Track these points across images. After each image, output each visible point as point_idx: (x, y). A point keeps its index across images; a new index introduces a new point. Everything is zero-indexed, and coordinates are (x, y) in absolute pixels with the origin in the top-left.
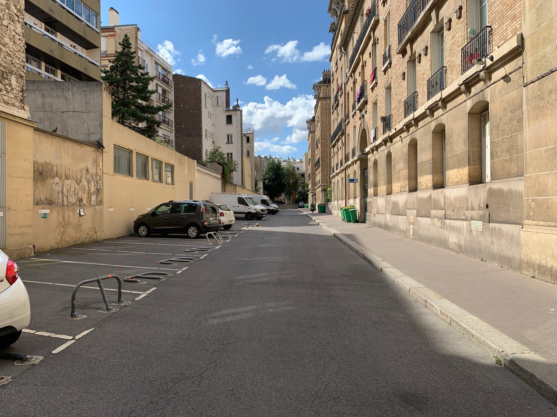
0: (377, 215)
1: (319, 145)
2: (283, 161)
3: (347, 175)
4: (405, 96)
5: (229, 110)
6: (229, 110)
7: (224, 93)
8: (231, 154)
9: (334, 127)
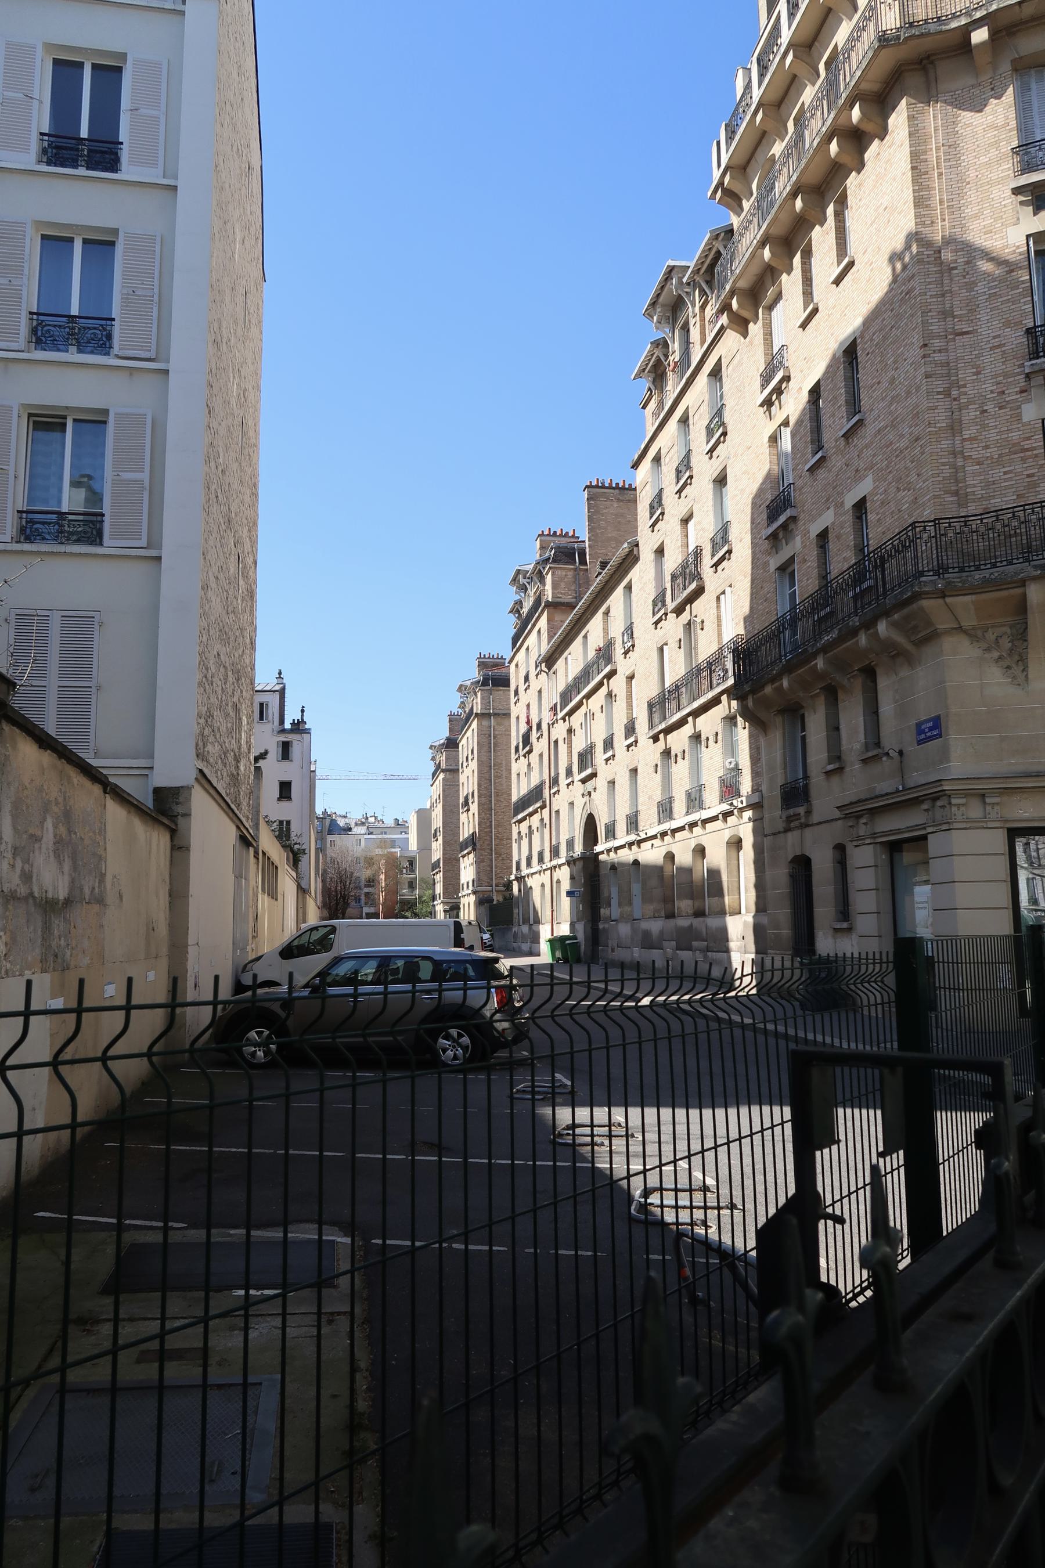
3: (555, 880)
4: (658, 796)
7: (277, 696)
8: (288, 822)
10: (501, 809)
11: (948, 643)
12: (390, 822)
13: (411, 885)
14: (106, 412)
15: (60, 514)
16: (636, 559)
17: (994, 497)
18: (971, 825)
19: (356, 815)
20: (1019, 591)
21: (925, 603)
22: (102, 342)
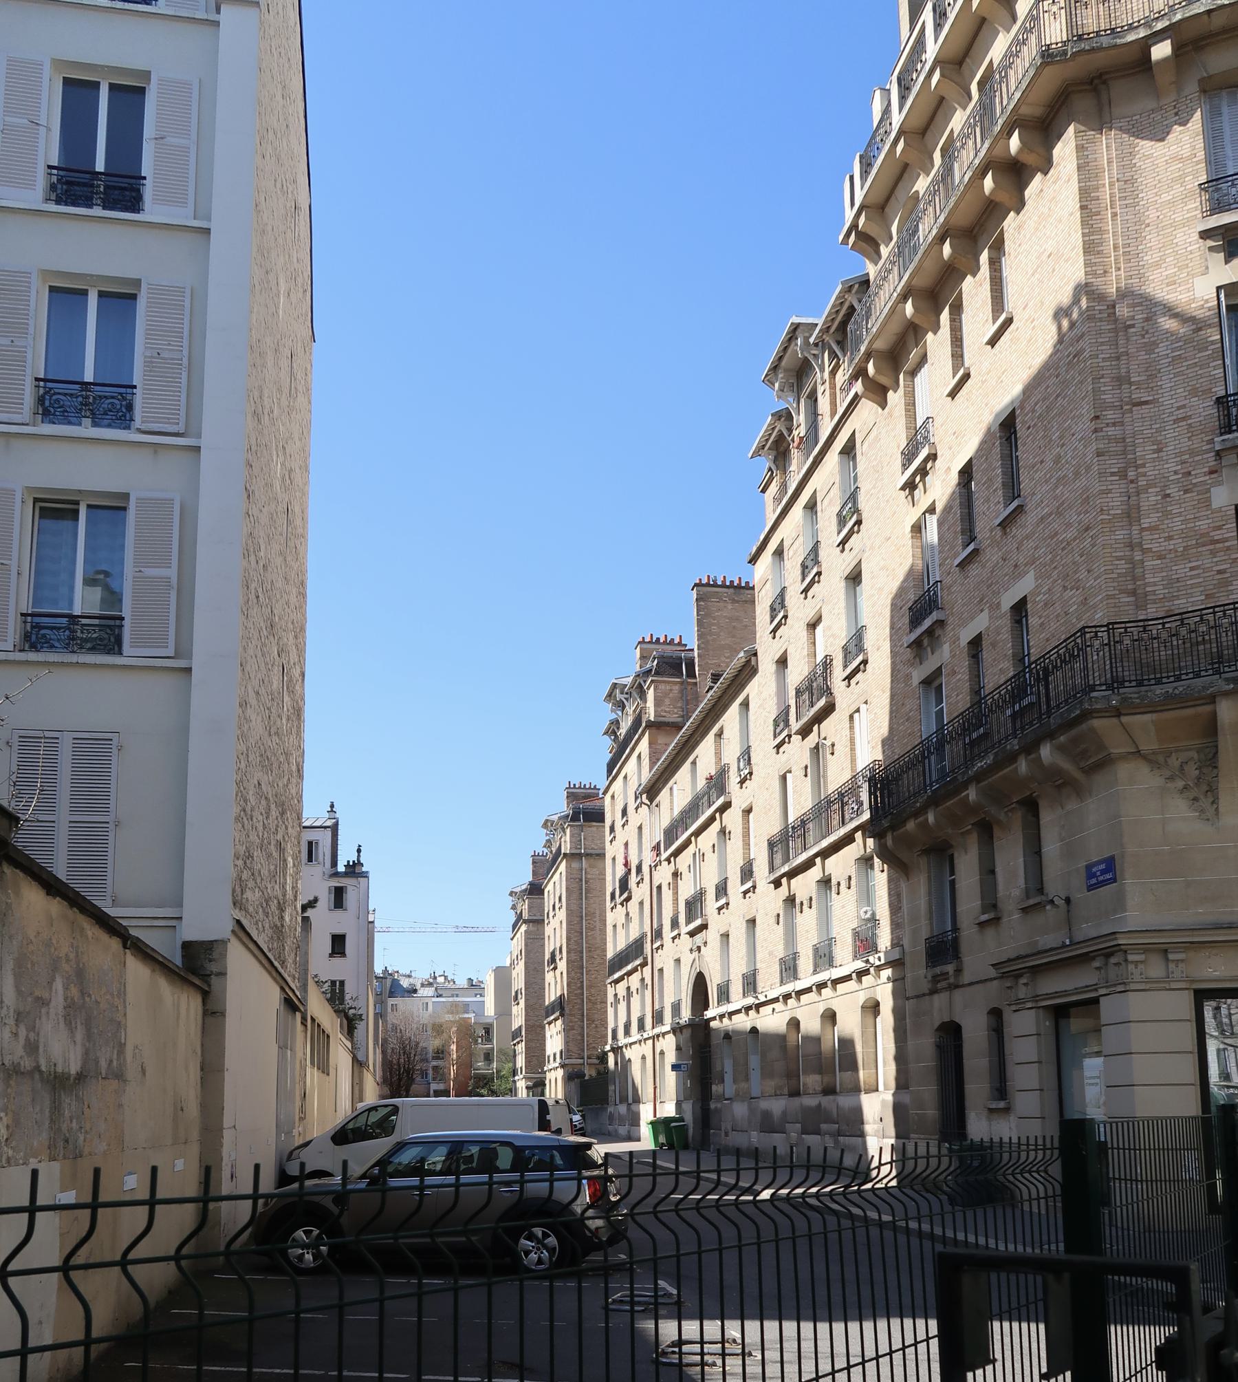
0: (733, 1135)
4: (780, 952)
5: (336, 874)
6: (336, 874)
7: (329, 833)
8: (342, 983)
11: (1123, 770)
12: (462, 982)
13: (488, 1057)
15: (73, 618)
17: (1178, 598)
18: (1152, 985)
19: (422, 974)
21: (1096, 723)
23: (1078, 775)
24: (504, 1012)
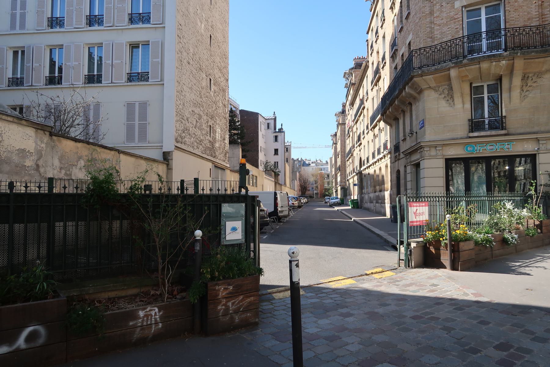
1: (340, 156)
2: (312, 163)
6: (276, 132)
7: (273, 120)
9: (347, 150)
10: (346, 155)
11: (426, 93)
12: (324, 162)
13: (328, 183)
14: (149, 41)
15: (138, 73)
16: (368, 67)
17: (444, 38)
18: (431, 157)
19: (313, 160)
20: (448, 72)
21: (415, 79)
22: (148, 21)
23: (416, 95)
24: (331, 171)
